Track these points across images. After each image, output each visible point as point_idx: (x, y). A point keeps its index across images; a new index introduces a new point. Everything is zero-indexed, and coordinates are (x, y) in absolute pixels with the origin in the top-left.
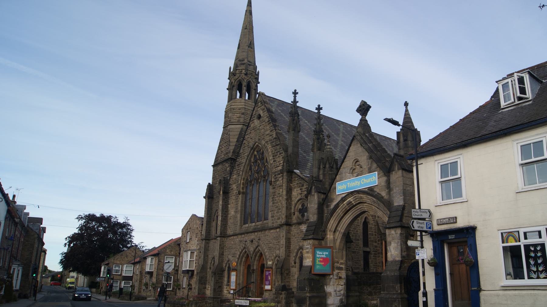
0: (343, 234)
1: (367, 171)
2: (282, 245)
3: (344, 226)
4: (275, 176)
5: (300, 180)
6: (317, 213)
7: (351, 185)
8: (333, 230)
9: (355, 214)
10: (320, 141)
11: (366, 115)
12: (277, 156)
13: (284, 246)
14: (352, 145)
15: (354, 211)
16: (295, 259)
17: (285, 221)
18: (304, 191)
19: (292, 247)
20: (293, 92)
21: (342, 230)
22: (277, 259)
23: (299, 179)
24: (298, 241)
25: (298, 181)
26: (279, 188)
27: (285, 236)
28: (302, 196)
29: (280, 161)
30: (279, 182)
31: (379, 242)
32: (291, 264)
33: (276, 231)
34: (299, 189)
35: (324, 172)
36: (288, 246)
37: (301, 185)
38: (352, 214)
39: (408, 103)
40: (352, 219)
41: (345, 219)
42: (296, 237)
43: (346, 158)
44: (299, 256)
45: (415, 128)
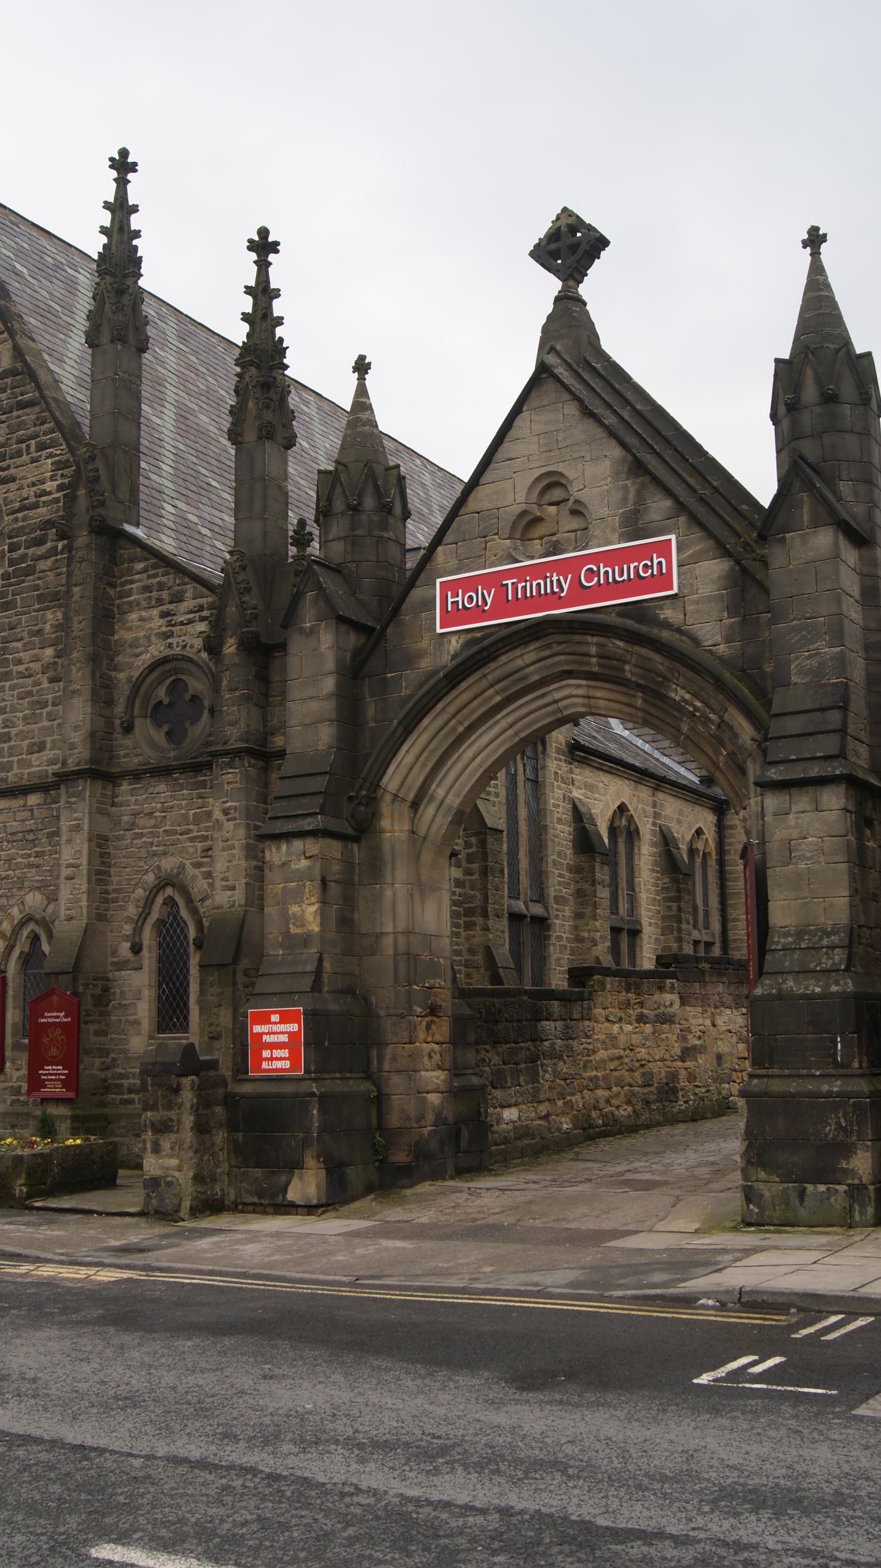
0: (456, 813)
2: (69, 866)
3: (461, 780)
4: (13, 548)
5: (160, 571)
6: (333, 715)
7: (524, 588)
8: (411, 797)
9: (529, 725)
10: (272, 394)
11: (582, 282)
12: (25, 458)
13: (85, 872)
14: (525, 408)
15: (524, 711)
16: (138, 930)
17: (87, 755)
18: (182, 623)
19: (115, 879)
20: (112, 159)
21: (450, 797)
22: (32, 931)
23: (155, 566)
24: (154, 848)
25: (149, 577)
26: (37, 606)
27: (86, 827)
29: (43, 482)
30: (39, 578)
31: (475, 866)
32: (114, 953)
33: (21, 802)
34: (155, 612)
35: (353, 528)
36: (98, 873)
37: (165, 595)
39: (369, 364)
40: (503, 749)
41: (474, 748)
42: (137, 831)
43: (492, 466)
44: (155, 915)
45: (859, 349)
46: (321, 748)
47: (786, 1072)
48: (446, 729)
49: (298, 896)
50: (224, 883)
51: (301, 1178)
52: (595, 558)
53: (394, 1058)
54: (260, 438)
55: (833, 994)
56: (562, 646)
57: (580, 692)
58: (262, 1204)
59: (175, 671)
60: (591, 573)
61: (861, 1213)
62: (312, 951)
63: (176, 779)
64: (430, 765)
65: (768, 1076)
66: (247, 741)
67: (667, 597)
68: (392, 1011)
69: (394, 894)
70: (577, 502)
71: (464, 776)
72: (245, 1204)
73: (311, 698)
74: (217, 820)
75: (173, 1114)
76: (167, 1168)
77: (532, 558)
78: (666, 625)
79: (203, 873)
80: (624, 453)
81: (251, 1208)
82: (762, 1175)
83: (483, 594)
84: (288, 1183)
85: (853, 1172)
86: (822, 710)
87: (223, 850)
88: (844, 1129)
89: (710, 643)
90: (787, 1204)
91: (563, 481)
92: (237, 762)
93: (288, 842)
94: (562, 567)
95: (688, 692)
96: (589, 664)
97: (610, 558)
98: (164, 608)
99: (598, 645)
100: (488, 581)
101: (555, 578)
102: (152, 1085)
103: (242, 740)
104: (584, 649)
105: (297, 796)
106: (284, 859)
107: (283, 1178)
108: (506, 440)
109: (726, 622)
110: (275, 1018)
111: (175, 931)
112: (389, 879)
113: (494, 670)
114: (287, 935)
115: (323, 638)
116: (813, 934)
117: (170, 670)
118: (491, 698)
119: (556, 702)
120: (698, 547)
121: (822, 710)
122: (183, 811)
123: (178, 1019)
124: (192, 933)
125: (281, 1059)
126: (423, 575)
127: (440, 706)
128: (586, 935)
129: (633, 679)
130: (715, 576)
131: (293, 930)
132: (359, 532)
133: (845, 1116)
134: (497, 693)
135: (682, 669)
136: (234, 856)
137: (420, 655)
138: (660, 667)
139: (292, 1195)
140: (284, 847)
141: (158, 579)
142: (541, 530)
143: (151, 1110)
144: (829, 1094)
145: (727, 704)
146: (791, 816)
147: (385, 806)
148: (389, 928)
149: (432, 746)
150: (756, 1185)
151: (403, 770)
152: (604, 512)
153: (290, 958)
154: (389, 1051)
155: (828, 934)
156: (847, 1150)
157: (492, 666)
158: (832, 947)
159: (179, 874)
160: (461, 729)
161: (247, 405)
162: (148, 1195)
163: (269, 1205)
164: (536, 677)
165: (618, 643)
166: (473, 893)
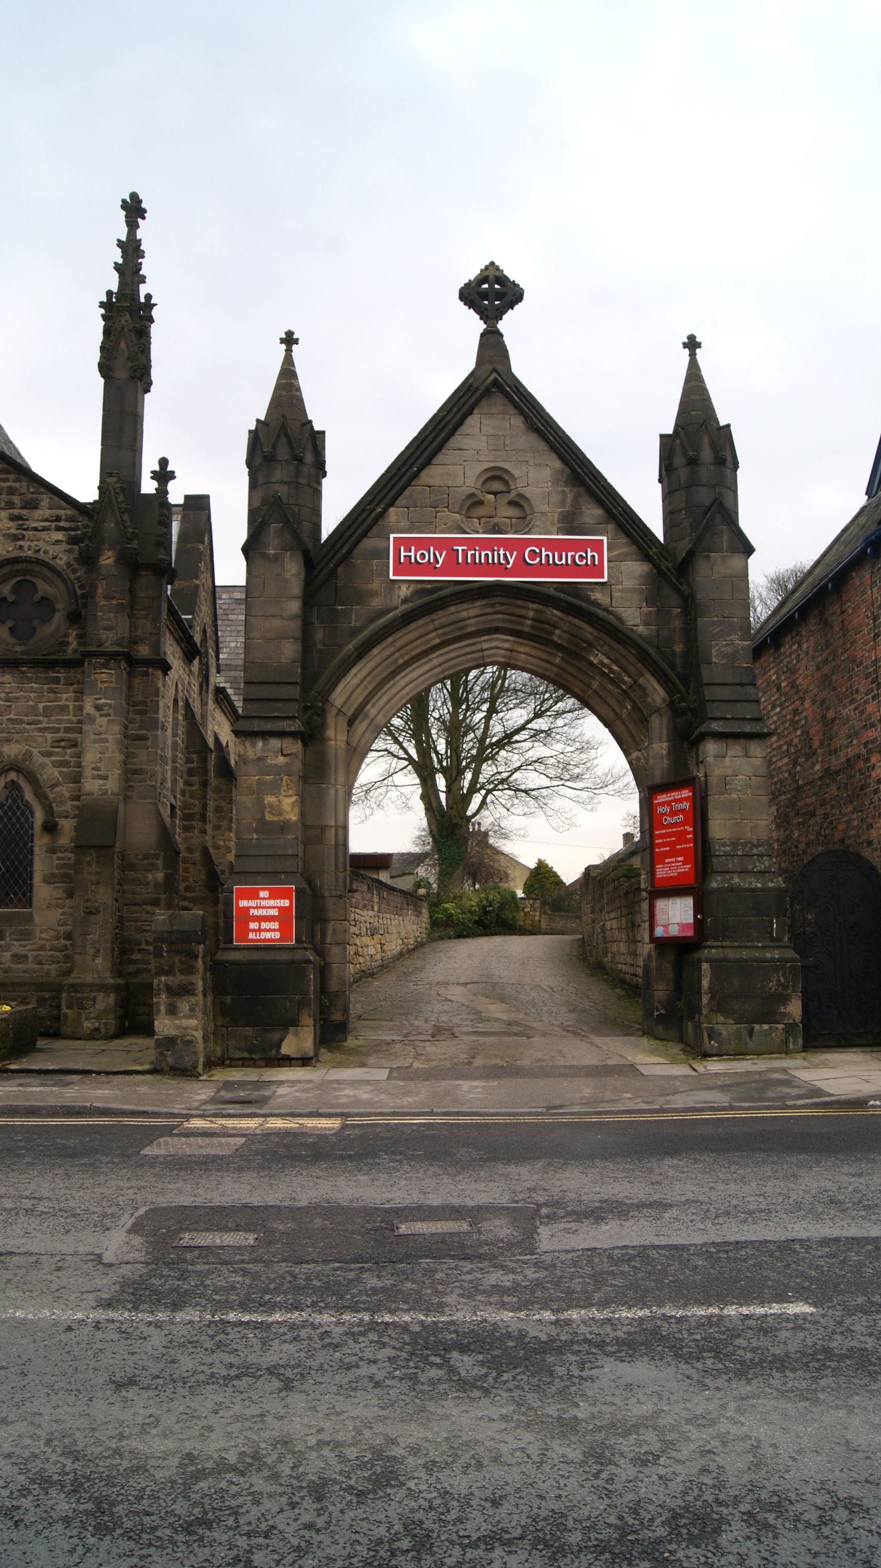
1: (553, 524)
5: (11, 477)
7: (474, 556)
8: (350, 713)
14: (475, 412)
15: (454, 654)
18: (35, 529)
21: (380, 717)
28: (21, 547)
31: (195, 779)
35: (297, 476)
38: (440, 665)
41: (407, 679)
43: (444, 451)
46: (284, 660)
47: (736, 944)
48: (390, 660)
49: (275, 788)
50: (96, 773)
51: (296, 1034)
52: (539, 543)
53: (334, 932)
54: (132, 377)
55: (771, 889)
56: (504, 607)
57: (506, 645)
58: (252, 1059)
59: (25, 572)
60: (533, 554)
61: (794, 1044)
62: (289, 837)
63: (23, 672)
64: (370, 688)
65: (722, 947)
66: (122, 646)
67: (597, 583)
68: (334, 893)
69: (336, 791)
70: (520, 495)
71: (393, 701)
72: (232, 1059)
73: (274, 616)
74: (89, 715)
75: (190, 978)
76: (186, 1029)
77: (477, 532)
78: (596, 604)
79: (53, 762)
80: (563, 466)
81: (240, 1062)
82: (721, 1019)
83: (435, 554)
84: (282, 1039)
85: (789, 1015)
86: (742, 685)
87: (95, 742)
88: (783, 985)
89: (631, 623)
90: (740, 1040)
91: (506, 477)
92: (113, 663)
93: (264, 739)
94: (509, 545)
95: (608, 658)
96: (523, 624)
97: (551, 545)
98: (16, 512)
99: (535, 610)
100: (440, 544)
101: (502, 552)
102: (168, 952)
103: (118, 645)
104: (523, 612)
105: (268, 700)
106: (259, 754)
107: (277, 1035)
108: (458, 433)
109: (646, 609)
110: (262, 894)
111: (14, 814)
112: (333, 781)
113: (441, 617)
114: (262, 822)
115: (287, 566)
116: (744, 845)
117: (18, 571)
118: (432, 639)
119: (482, 650)
120: (623, 550)
121: (742, 685)
122: (31, 703)
123: (16, 895)
124: (39, 817)
125: (270, 930)
126: (375, 528)
127: (390, 639)
128: (222, 843)
129: (559, 641)
130: (637, 574)
131: (268, 817)
132: (302, 481)
133: (784, 975)
134: (438, 636)
135: (608, 640)
136: (107, 748)
137: (371, 594)
138: (589, 636)
139: (287, 1048)
140: (260, 744)
141: (9, 484)
142: (480, 511)
143: (166, 973)
144: (772, 960)
145: (644, 671)
146: (727, 759)
147: (331, 718)
148: (333, 823)
149: (376, 672)
150: (716, 1026)
151: (349, 690)
152: (544, 508)
153: (266, 842)
154: (330, 926)
155: (756, 846)
156: (784, 999)
157: (441, 613)
158: (761, 856)
159: (24, 760)
160: (401, 661)
161: (119, 345)
162: (161, 1054)
163: (261, 1059)
164: (473, 629)
165: (555, 612)
166: (192, 801)
